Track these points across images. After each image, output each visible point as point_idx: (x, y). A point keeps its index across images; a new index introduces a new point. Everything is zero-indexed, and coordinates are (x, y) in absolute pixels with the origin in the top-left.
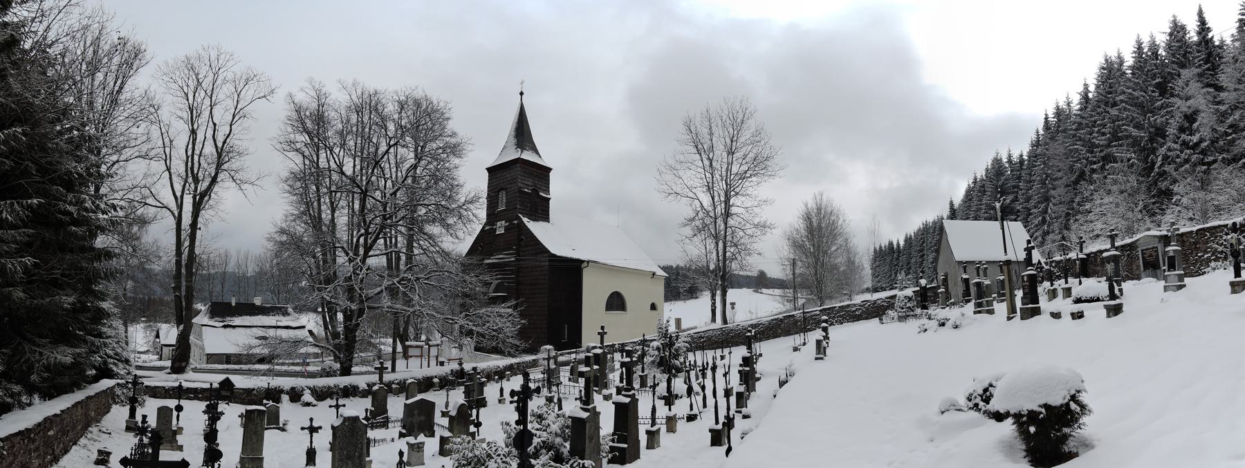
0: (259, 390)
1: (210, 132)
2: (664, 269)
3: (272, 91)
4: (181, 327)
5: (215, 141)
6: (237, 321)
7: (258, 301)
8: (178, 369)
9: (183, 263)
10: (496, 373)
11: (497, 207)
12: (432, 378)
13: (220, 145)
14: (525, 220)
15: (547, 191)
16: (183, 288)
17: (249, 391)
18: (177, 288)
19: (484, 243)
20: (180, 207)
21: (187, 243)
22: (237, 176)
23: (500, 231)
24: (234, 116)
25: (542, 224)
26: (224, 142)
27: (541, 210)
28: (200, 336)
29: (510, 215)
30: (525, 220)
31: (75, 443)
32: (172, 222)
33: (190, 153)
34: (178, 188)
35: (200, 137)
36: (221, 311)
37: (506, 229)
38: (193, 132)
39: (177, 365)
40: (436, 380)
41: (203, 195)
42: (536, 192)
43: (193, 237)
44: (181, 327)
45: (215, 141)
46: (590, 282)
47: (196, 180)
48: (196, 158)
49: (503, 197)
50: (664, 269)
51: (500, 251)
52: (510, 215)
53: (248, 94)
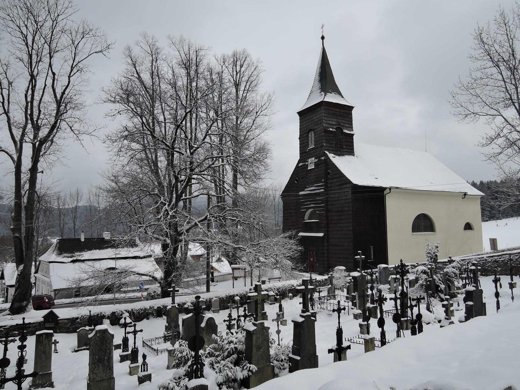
0: (83, 318)
1: (49, 82)
2: (481, 186)
3: (108, 47)
4: (21, 267)
5: (54, 90)
6: (87, 255)
7: (107, 236)
8: (16, 309)
9: (23, 205)
10: (290, 291)
11: (308, 146)
12: (233, 296)
13: (59, 97)
14: (331, 156)
15: (351, 128)
16: (23, 230)
17: (73, 321)
18: (17, 229)
19: (299, 177)
20: (20, 151)
21: (27, 186)
22: (76, 126)
23: (311, 167)
24: (72, 68)
25: (347, 158)
26: (63, 93)
27: (346, 146)
28: (47, 273)
29: (318, 152)
30: (331, 156)
31: (39, 156)
32: (12, 166)
33: (29, 99)
34: (17, 133)
35: (40, 84)
36: (69, 247)
37: (316, 164)
38: (33, 77)
39: (16, 305)
40: (237, 298)
41: (43, 142)
42: (340, 130)
43: (33, 181)
44: (21, 267)
45: (54, 90)
46: (391, 204)
47: (37, 128)
48: (36, 104)
49: (312, 135)
50: (481, 186)
51: (311, 184)
52: (318, 152)
53: (86, 46)
